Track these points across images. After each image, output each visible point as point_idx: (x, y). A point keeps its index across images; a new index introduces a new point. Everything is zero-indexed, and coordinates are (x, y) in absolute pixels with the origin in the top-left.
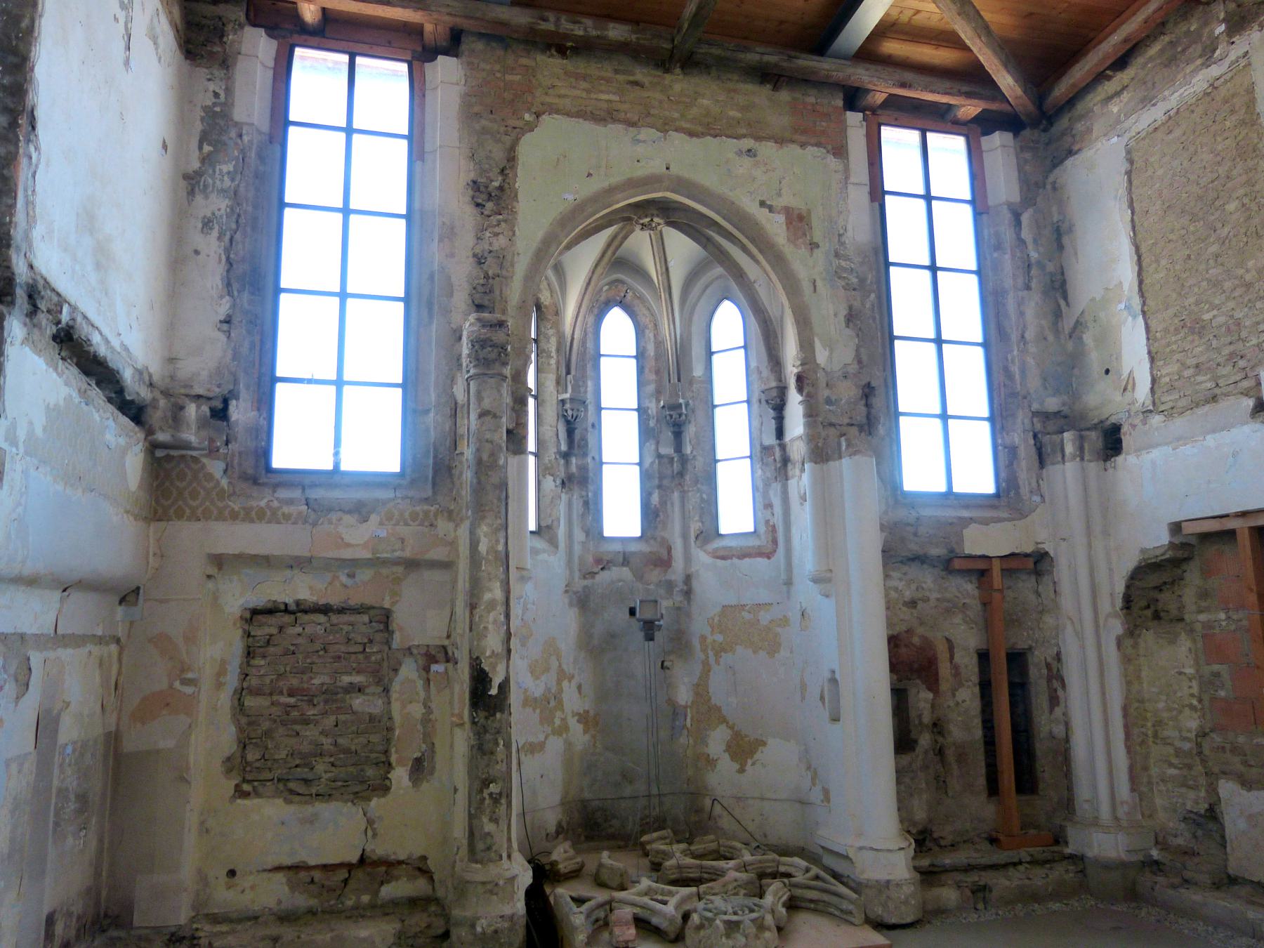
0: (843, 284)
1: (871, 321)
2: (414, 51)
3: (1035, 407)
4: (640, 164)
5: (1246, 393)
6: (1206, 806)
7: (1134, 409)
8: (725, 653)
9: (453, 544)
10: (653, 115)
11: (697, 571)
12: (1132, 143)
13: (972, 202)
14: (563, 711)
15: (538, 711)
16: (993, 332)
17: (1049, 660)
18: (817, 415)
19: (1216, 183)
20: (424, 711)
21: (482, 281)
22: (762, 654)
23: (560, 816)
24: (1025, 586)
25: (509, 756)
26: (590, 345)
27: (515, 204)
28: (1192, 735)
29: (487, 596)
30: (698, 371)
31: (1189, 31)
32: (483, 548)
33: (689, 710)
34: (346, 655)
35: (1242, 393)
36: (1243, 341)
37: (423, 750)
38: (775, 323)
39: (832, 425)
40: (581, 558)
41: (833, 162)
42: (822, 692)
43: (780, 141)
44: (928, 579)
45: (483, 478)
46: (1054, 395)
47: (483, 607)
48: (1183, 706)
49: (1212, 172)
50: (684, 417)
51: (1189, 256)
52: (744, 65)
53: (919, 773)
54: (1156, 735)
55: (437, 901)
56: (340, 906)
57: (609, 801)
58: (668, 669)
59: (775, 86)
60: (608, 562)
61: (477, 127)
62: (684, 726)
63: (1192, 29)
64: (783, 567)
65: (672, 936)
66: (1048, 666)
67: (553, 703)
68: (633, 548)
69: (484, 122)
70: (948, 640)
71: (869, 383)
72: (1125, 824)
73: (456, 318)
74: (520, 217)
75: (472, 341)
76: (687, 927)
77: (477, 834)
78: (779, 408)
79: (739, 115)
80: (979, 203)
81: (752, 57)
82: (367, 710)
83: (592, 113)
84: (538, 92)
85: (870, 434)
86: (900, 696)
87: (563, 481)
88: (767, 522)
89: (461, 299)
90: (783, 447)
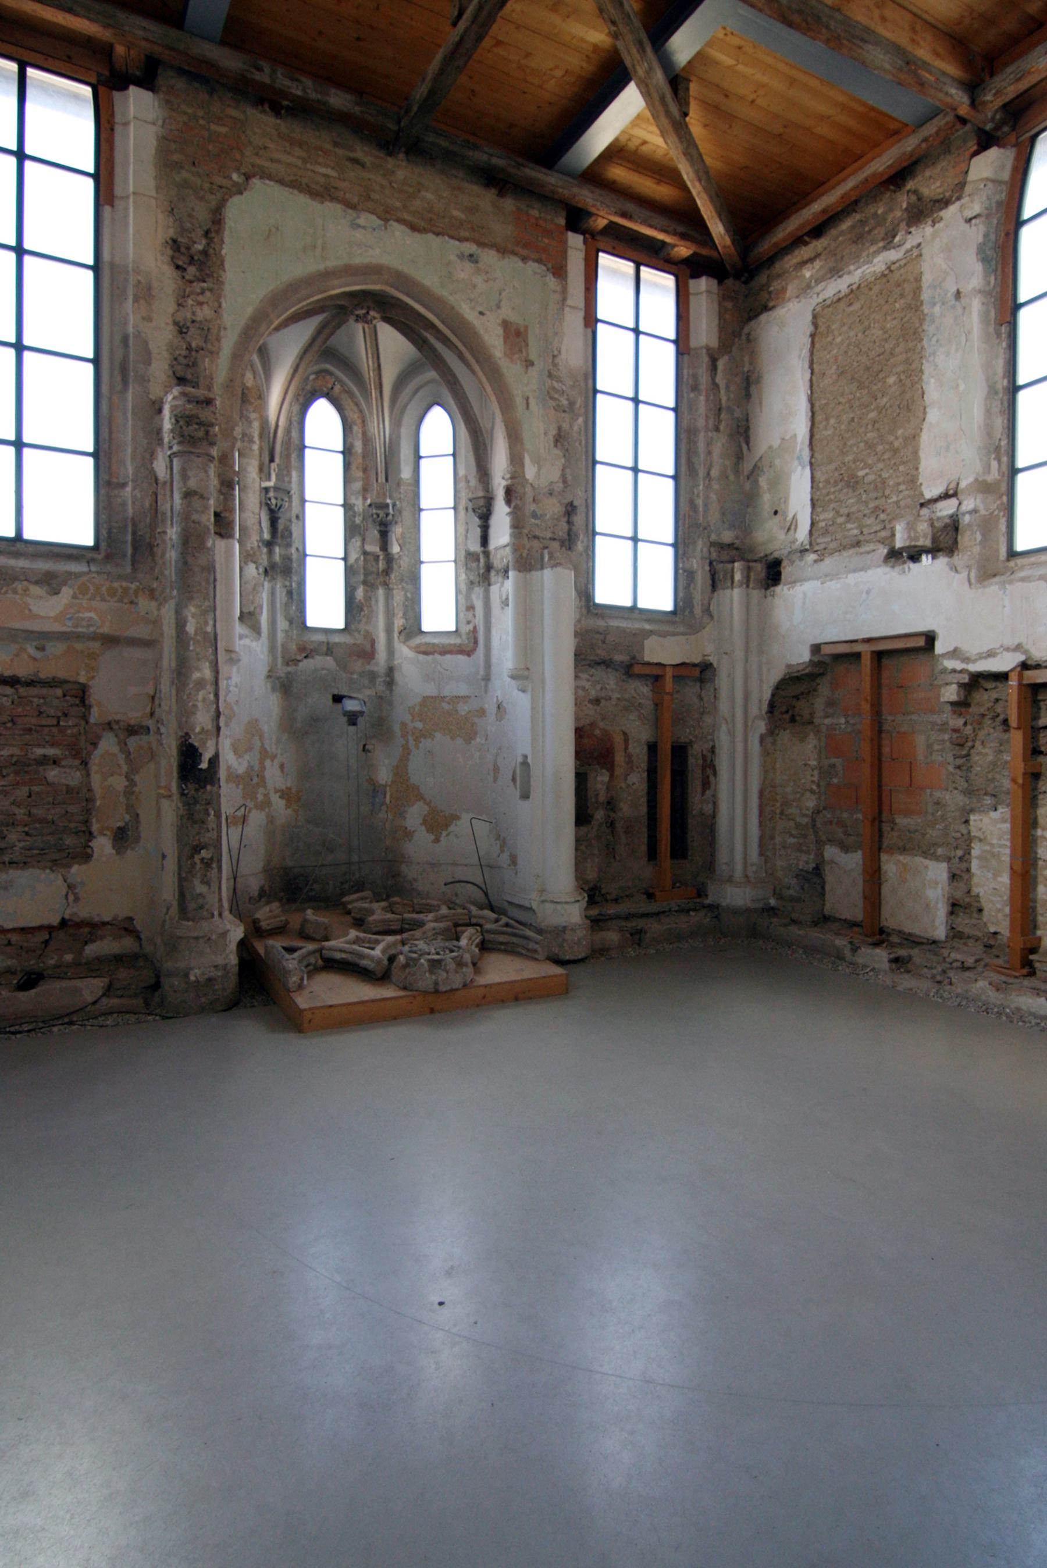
0: (554, 404)
1: (577, 444)
2: (99, 75)
3: (713, 537)
5: (882, 542)
6: (814, 865)
7: (794, 547)
9: (156, 623)
10: (373, 200)
11: (400, 664)
12: (818, 309)
14: (265, 787)
15: (241, 787)
16: (684, 469)
17: (705, 752)
18: (523, 527)
19: (881, 357)
21: (184, 353)
22: (459, 741)
23: (263, 882)
24: (691, 692)
25: (219, 826)
26: (294, 434)
27: (221, 273)
28: (809, 813)
29: (196, 675)
30: (406, 474)
31: (876, 214)
32: (190, 628)
33: (388, 788)
34: (38, 728)
35: (879, 541)
36: (886, 497)
37: (127, 820)
40: (284, 646)
41: (552, 281)
42: (514, 773)
43: (503, 251)
44: (611, 680)
45: (190, 560)
46: (729, 529)
48: (806, 790)
49: (879, 347)
50: (390, 517)
51: (853, 420)
54: (782, 813)
55: (145, 957)
56: (41, 965)
59: (500, 191)
60: (311, 651)
62: (384, 803)
63: (879, 212)
64: (482, 663)
65: (379, 975)
66: (704, 758)
67: (255, 780)
68: (337, 639)
69: (184, 174)
70: (625, 734)
71: (572, 502)
72: (752, 880)
73: (155, 390)
74: (227, 288)
75: (176, 416)
76: (393, 967)
77: (188, 896)
78: (485, 517)
79: (460, 215)
80: (682, 342)
81: (480, 157)
82: (63, 781)
83: (307, 185)
84: (248, 151)
85: (570, 549)
86: (581, 779)
89: (160, 369)
90: (487, 554)
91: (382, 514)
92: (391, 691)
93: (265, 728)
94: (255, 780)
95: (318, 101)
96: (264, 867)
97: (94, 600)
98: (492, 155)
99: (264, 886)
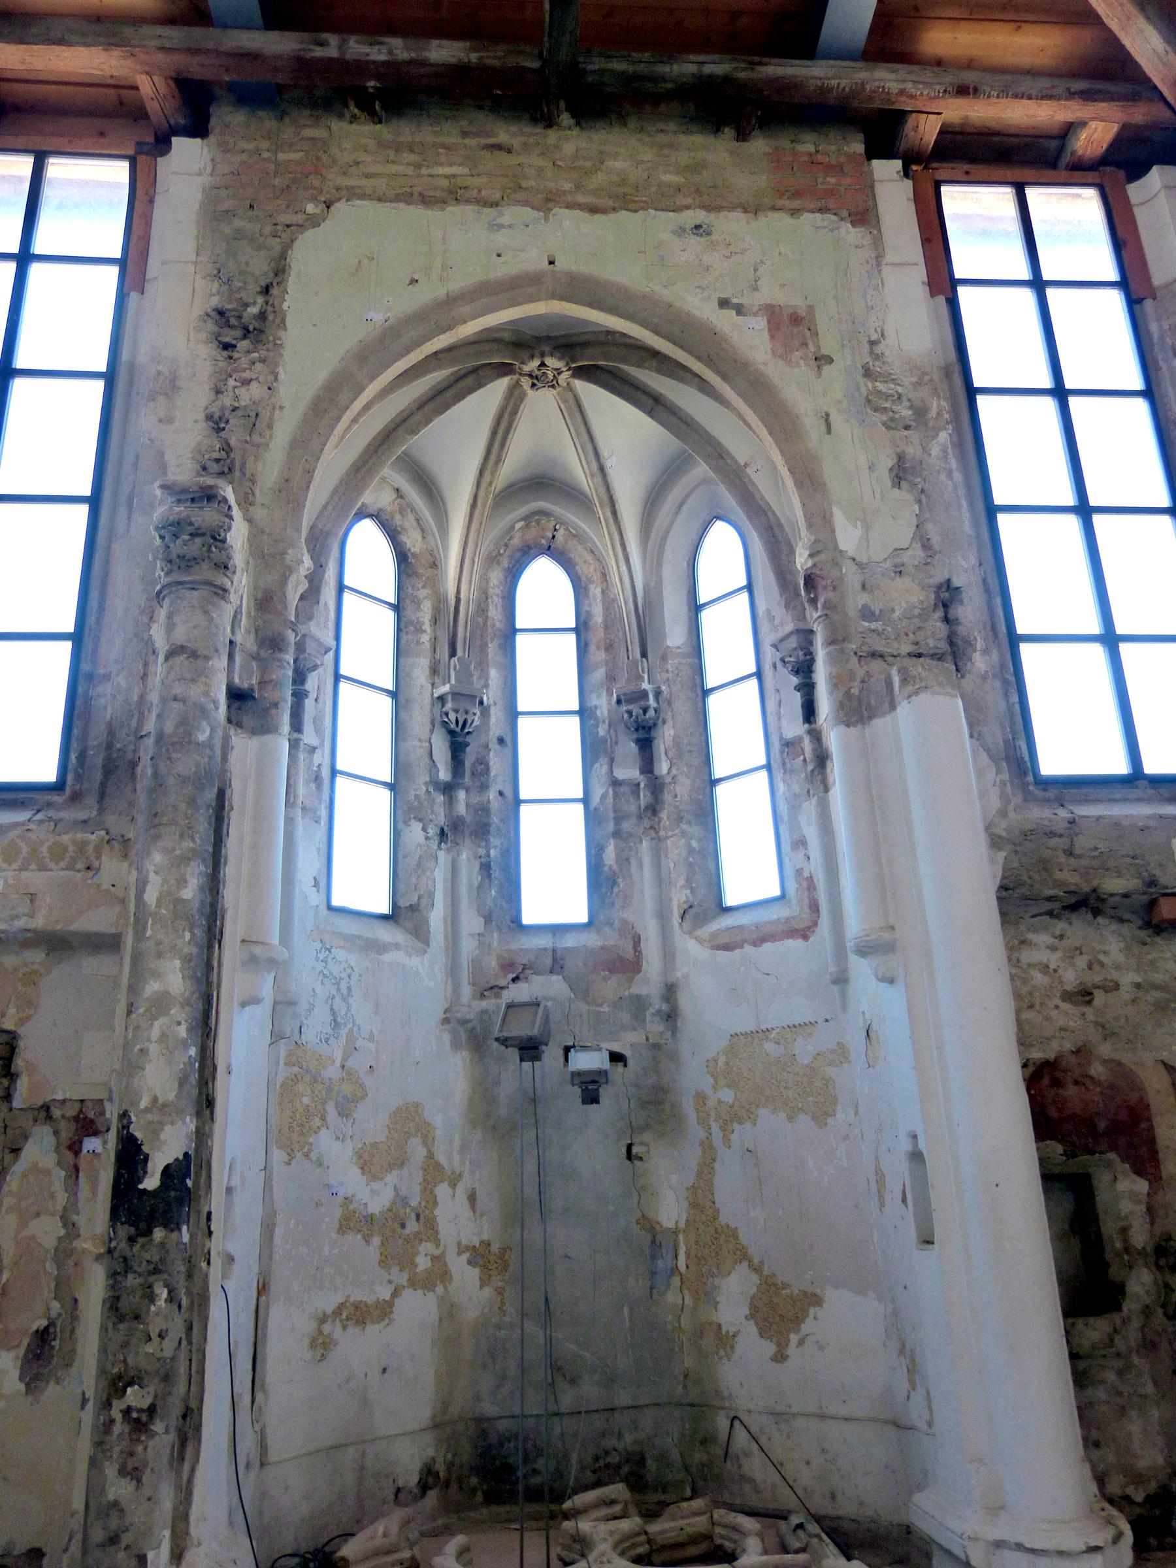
1: (943, 477)
4: (501, 259)
8: (740, 1123)
10: (526, 189)
11: (685, 976)
13: (1123, 284)
14: (437, 1242)
15: (376, 1241)
20: (63, 1232)
21: (216, 455)
22: (804, 1120)
23: (431, 1452)
26: (495, 612)
27: (281, 333)
29: (152, 987)
30: (675, 637)
33: (681, 1237)
38: (787, 529)
39: (875, 655)
40: (476, 964)
41: (851, 234)
43: (753, 209)
45: (162, 767)
47: (141, 1010)
50: (651, 713)
52: (669, 86)
53: (1136, 1360)
57: (532, 1421)
58: (641, 1159)
60: (525, 967)
61: (227, 230)
62: (675, 1270)
67: (412, 1227)
68: (570, 941)
69: (238, 223)
71: (949, 581)
74: (288, 352)
87: (442, 830)
88: (799, 872)
91: (636, 709)
92: (674, 1031)
93: (438, 1120)
94: (412, 1227)
95: (411, 62)
96: (434, 1417)
97: (27, 870)
98: (703, 63)
99: (434, 1460)
